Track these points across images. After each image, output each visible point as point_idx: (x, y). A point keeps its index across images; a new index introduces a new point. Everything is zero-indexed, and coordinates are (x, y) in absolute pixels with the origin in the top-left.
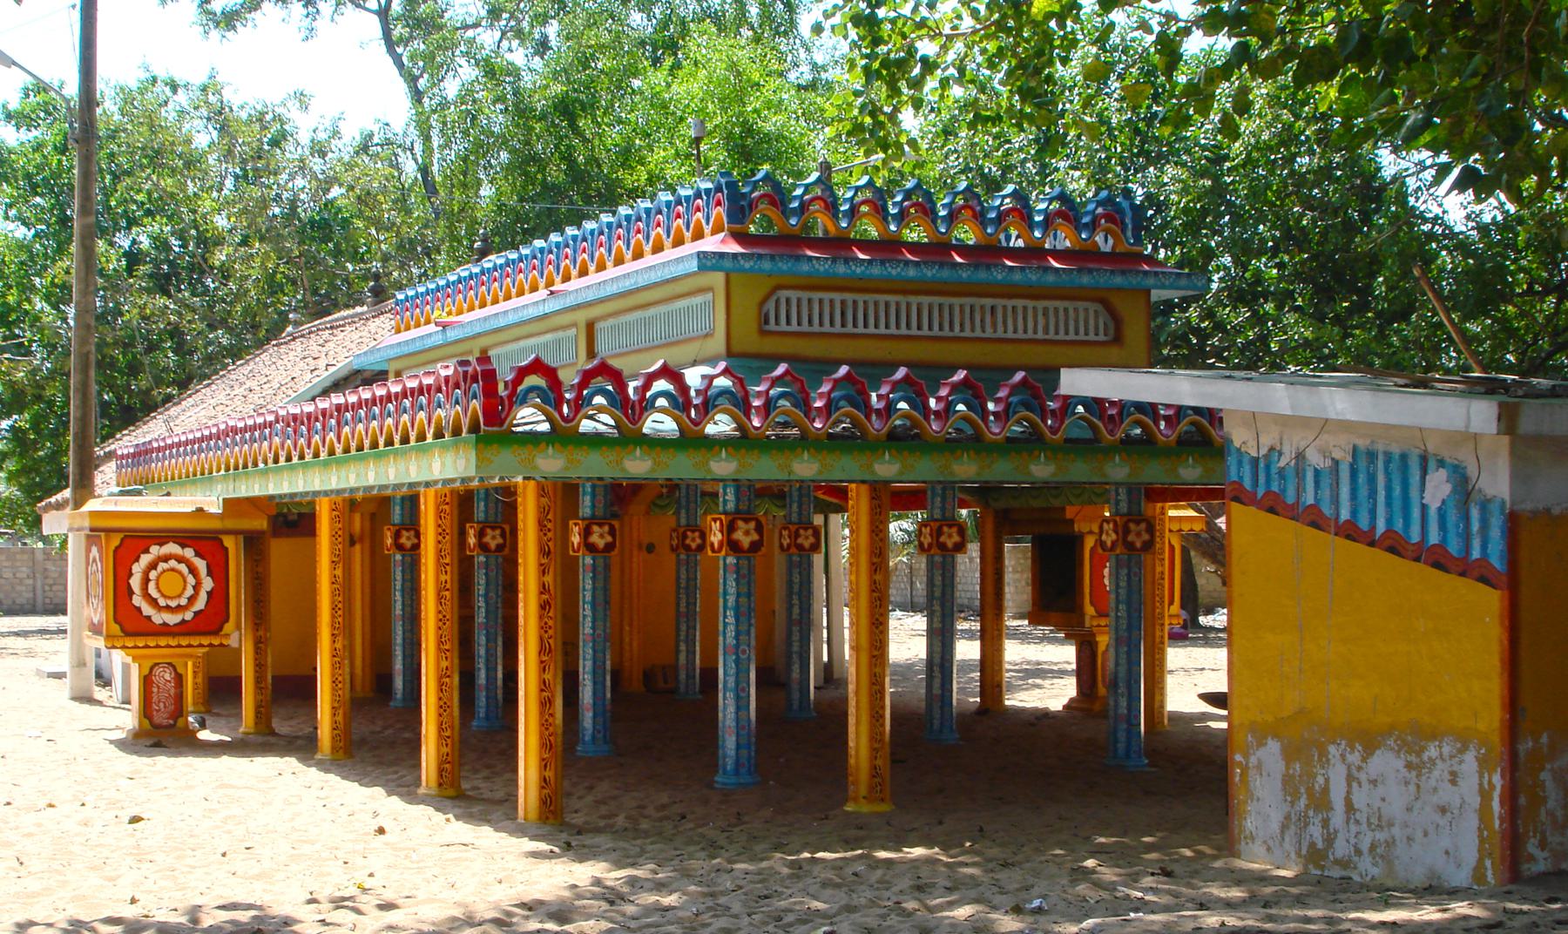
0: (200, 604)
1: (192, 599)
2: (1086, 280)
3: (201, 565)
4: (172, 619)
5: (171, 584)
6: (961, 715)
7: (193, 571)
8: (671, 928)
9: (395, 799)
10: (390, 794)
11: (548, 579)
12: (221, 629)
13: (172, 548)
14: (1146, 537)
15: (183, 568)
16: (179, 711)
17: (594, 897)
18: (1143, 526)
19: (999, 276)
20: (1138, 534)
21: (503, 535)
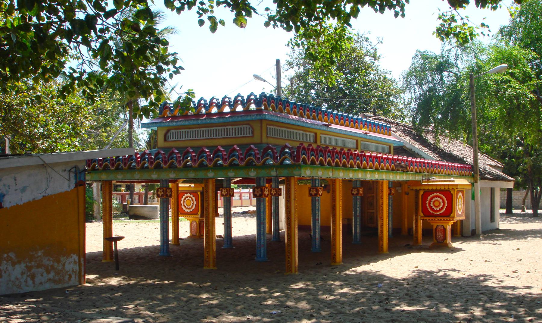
0: (194, 208)
1: (192, 206)
2: (187, 123)
3: (194, 198)
4: (189, 211)
5: (188, 202)
6: (218, 242)
7: (192, 200)
8: (511, 320)
9: (371, 264)
10: (369, 264)
11: (381, 202)
12: (450, 215)
13: (188, 195)
14: (260, 193)
15: (190, 199)
16: (445, 238)
17: (423, 301)
18: (259, 189)
19: (213, 121)
20: (258, 192)
21: (163, 191)
